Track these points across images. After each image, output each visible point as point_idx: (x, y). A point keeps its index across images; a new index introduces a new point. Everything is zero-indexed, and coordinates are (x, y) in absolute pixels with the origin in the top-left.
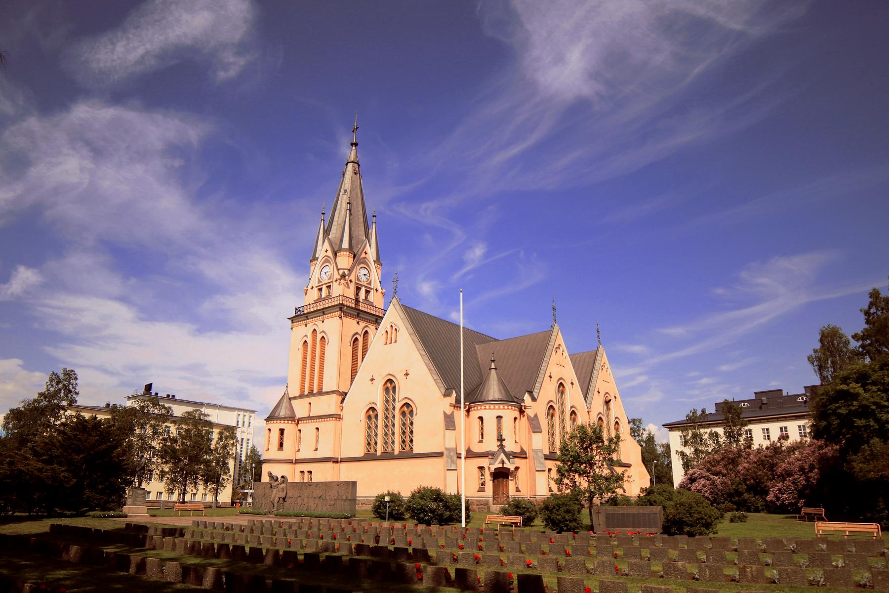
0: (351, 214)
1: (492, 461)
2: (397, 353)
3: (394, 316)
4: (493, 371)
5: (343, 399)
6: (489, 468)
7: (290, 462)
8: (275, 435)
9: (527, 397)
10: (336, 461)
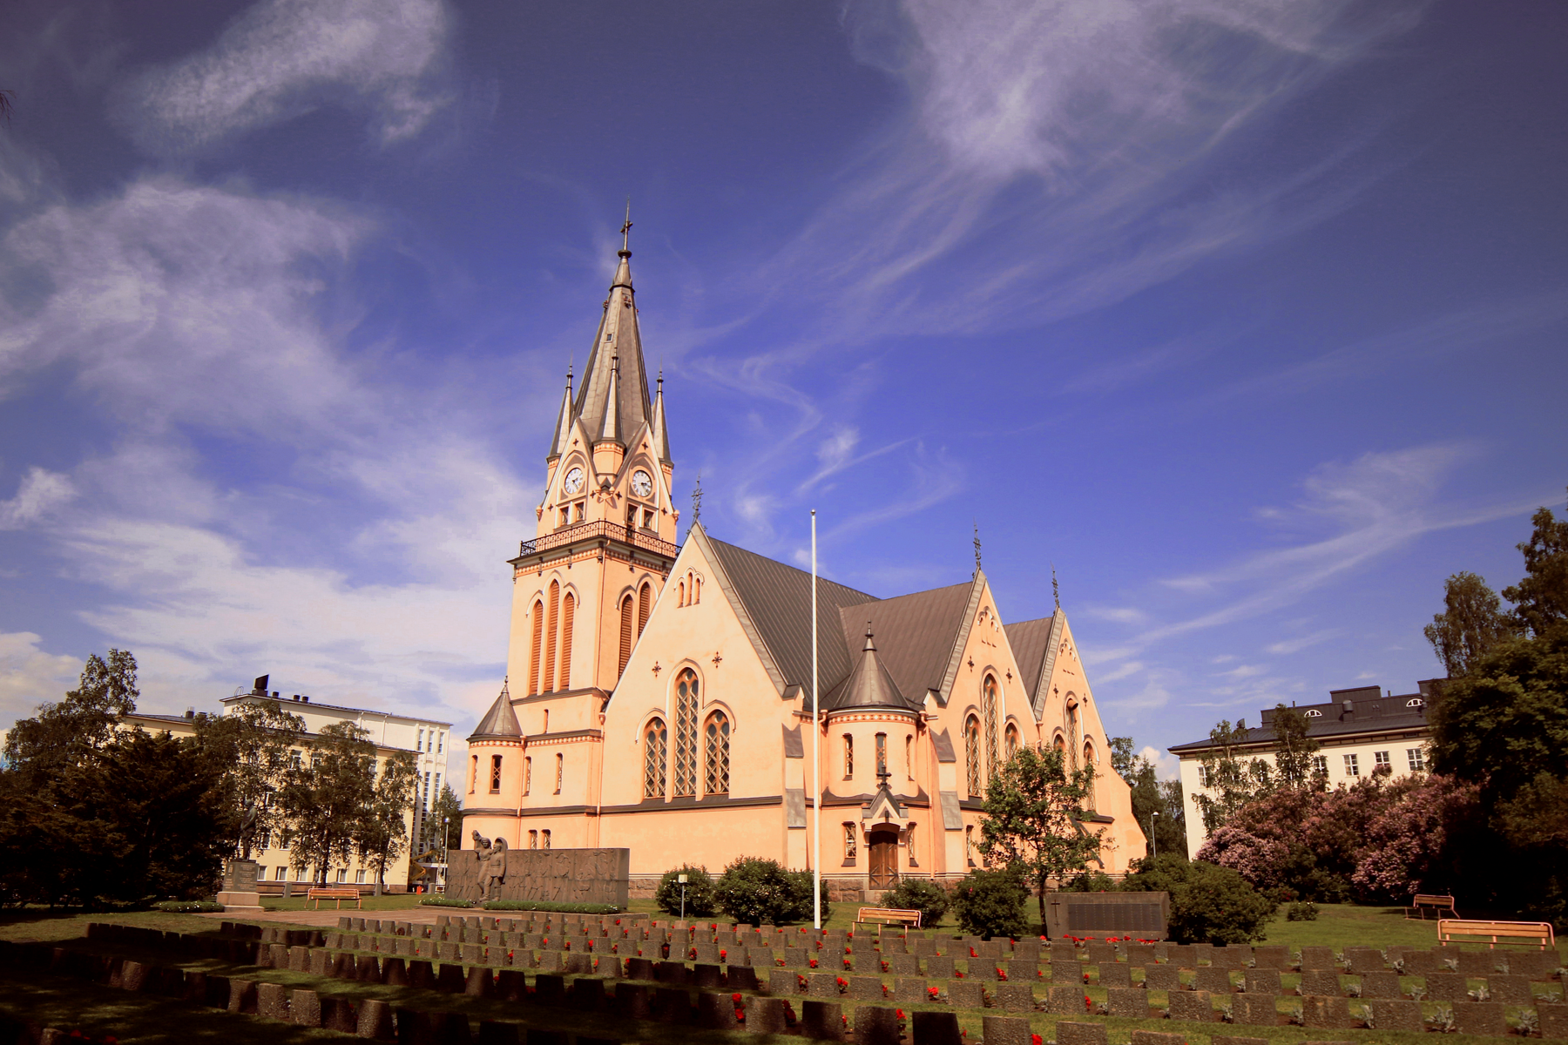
0: (619, 378)
1: (868, 812)
2: (700, 622)
3: (694, 557)
4: (870, 655)
5: (606, 704)
6: (863, 826)
7: (512, 814)
8: (486, 766)
9: (929, 700)
10: (592, 812)
